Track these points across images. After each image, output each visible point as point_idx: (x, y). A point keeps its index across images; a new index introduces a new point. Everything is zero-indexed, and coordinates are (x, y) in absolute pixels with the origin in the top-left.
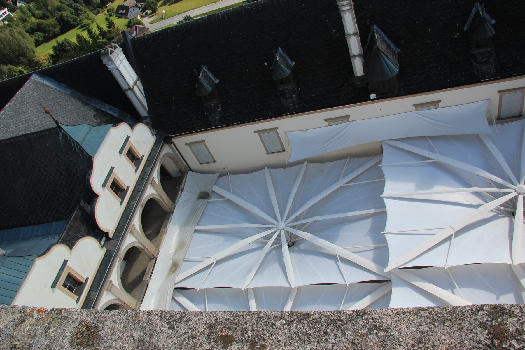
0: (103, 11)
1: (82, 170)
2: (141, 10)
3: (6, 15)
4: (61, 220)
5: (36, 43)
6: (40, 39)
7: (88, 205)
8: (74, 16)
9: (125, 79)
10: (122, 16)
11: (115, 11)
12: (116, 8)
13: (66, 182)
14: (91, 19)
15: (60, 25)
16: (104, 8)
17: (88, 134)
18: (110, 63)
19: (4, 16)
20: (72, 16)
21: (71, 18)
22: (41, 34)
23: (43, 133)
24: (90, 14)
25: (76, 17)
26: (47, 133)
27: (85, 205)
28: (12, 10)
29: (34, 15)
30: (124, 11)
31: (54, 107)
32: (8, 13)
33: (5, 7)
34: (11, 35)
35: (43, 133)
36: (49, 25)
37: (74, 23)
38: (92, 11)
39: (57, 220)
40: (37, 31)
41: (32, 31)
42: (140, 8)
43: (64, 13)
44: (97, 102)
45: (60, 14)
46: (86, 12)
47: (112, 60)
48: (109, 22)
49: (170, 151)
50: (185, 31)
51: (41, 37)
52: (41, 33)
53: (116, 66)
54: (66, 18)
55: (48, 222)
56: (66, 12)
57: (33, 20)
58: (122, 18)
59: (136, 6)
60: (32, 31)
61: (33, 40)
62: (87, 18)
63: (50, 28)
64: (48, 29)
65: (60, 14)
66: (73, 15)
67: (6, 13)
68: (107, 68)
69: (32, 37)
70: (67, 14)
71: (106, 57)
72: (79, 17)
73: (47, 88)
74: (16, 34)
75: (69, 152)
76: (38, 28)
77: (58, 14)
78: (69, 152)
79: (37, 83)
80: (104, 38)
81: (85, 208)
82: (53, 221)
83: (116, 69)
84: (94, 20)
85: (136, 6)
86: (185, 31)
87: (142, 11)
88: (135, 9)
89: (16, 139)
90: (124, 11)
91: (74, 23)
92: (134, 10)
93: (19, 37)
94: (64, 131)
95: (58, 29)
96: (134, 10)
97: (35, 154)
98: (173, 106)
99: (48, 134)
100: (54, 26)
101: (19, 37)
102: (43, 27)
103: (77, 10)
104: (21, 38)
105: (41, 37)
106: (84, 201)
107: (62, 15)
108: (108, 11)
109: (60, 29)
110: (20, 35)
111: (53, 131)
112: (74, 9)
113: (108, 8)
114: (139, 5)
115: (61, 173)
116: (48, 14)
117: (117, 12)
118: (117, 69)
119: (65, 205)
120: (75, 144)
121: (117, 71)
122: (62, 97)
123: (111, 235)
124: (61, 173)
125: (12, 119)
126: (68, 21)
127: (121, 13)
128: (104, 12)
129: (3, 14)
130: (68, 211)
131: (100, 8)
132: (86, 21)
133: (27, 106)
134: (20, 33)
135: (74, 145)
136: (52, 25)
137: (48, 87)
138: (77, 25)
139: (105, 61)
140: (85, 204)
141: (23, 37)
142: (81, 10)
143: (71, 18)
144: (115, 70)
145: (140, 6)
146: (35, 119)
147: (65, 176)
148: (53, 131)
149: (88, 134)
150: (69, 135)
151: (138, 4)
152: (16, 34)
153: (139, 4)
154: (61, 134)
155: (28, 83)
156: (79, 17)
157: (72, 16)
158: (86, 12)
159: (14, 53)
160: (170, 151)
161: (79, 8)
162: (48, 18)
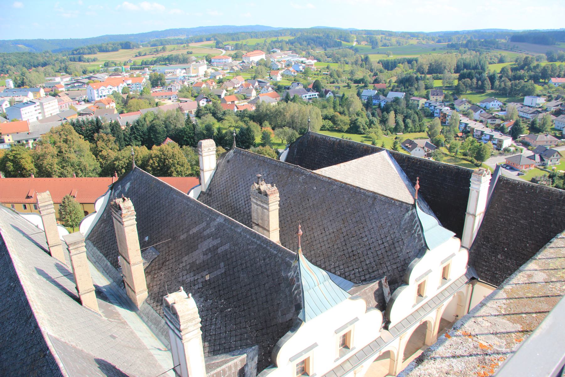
0: (391, 136)
1: (407, 253)
2: (426, 154)
3: (314, 96)
4: (350, 280)
5: (322, 127)
6: (327, 127)
7: (388, 286)
8: (366, 126)
9: (477, 204)
10: (406, 149)
11: (402, 141)
12: (405, 139)
13: (382, 253)
14: (378, 136)
15: (350, 125)
16: (394, 133)
17: (433, 227)
18: (476, 183)
19: (312, 97)
20: (365, 125)
21: (363, 126)
22: (331, 124)
23: (393, 201)
24: (380, 132)
25: (367, 128)
26: (397, 204)
27: (385, 284)
28: (321, 96)
29: (334, 108)
30: (410, 146)
31: (389, 187)
32: (316, 96)
33: (317, 92)
34: (310, 111)
35: (393, 201)
36: (341, 121)
37: (362, 130)
38: (383, 130)
39: (345, 278)
40: (330, 119)
41: (326, 118)
42: (425, 152)
43: (360, 119)
44: (426, 206)
45: (357, 117)
46: (377, 128)
47: (481, 182)
48: (394, 147)
49: (464, 292)
50: (562, 198)
51: (329, 126)
52: (332, 123)
53: (479, 189)
54: (359, 124)
55: (335, 273)
56: (362, 119)
57: (332, 110)
58: (405, 150)
59: (423, 148)
60: (326, 118)
61: (322, 124)
62: (375, 133)
63: (341, 123)
64: (339, 123)
65: (357, 117)
66: (366, 124)
67: (315, 95)
68: (470, 185)
69: (323, 121)
70: (362, 121)
71: (477, 177)
72: (369, 128)
73: (390, 168)
74: (314, 113)
75: (407, 231)
76: (332, 119)
77: (354, 117)
78: (407, 231)
79: (384, 159)
80: (117, 143)
81: (383, 286)
82: (340, 276)
83: (477, 191)
84: (380, 138)
85: (423, 148)
86: (562, 198)
87: (425, 155)
88: (421, 149)
89: (362, 191)
90: (410, 146)
91: (362, 130)
92: (419, 150)
93: (314, 116)
94: (416, 211)
95: (346, 128)
96: (419, 150)
97: (371, 212)
98: (500, 255)
99: (397, 204)
100: (345, 124)
101: (314, 116)
102: (336, 119)
103: (371, 122)
104: (315, 117)
105: (329, 126)
106: (386, 280)
107: (357, 120)
108: (396, 138)
109: (349, 128)
110: (316, 115)
111: (404, 204)
112: (370, 120)
113: (397, 136)
114: (426, 149)
115: (383, 243)
116: (346, 112)
117: (403, 144)
118: (478, 192)
119: (363, 271)
120: (418, 228)
121: (476, 193)
122: (399, 183)
123: (390, 326)
124: (383, 243)
125: (353, 173)
126: (359, 127)
127: (407, 146)
128: (391, 137)
129: (313, 95)
130: (363, 278)
131: (390, 132)
132: (372, 135)
133: (368, 171)
134: (317, 114)
135: (416, 229)
136: (344, 122)
137: (391, 167)
138: (364, 134)
139: (473, 179)
140: (386, 282)
141: (317, 118)
142: (374, 125)
143: (363, 126)
144: (475, 191)
145: (426, 151)
146: (370, 185)
147: (385, 247)
148: (404, 204)
149: (433, 227)
150: (418, 217)
151: (425, 148)
152: (314, 113)
153: (427, 148)
154: (410, 212)
155: (376, 155)
156: (369, 128)
157: (365, 125)
158: (377, 128)
159: (301, 125)
160: (464, 292)
161: (374, 122)
162: (345, 115)
